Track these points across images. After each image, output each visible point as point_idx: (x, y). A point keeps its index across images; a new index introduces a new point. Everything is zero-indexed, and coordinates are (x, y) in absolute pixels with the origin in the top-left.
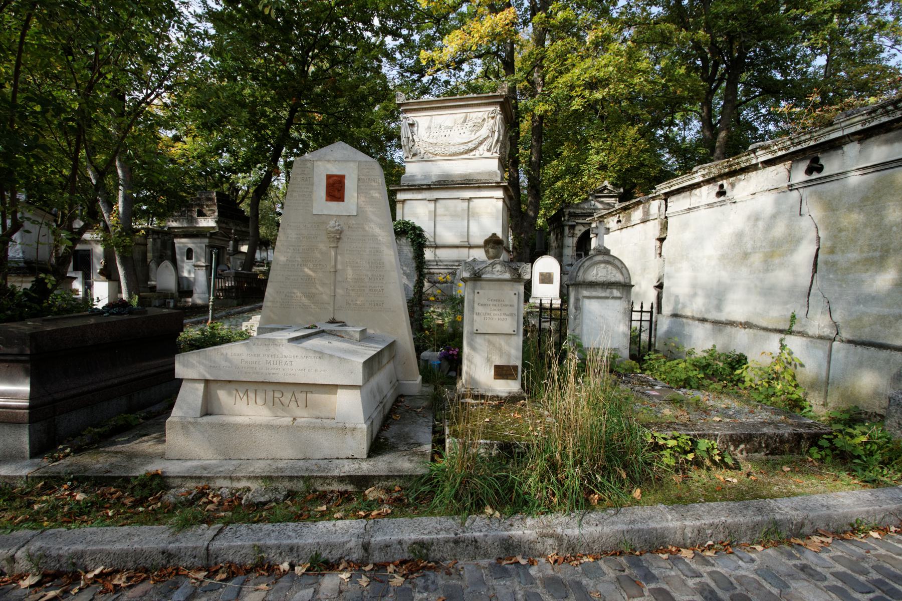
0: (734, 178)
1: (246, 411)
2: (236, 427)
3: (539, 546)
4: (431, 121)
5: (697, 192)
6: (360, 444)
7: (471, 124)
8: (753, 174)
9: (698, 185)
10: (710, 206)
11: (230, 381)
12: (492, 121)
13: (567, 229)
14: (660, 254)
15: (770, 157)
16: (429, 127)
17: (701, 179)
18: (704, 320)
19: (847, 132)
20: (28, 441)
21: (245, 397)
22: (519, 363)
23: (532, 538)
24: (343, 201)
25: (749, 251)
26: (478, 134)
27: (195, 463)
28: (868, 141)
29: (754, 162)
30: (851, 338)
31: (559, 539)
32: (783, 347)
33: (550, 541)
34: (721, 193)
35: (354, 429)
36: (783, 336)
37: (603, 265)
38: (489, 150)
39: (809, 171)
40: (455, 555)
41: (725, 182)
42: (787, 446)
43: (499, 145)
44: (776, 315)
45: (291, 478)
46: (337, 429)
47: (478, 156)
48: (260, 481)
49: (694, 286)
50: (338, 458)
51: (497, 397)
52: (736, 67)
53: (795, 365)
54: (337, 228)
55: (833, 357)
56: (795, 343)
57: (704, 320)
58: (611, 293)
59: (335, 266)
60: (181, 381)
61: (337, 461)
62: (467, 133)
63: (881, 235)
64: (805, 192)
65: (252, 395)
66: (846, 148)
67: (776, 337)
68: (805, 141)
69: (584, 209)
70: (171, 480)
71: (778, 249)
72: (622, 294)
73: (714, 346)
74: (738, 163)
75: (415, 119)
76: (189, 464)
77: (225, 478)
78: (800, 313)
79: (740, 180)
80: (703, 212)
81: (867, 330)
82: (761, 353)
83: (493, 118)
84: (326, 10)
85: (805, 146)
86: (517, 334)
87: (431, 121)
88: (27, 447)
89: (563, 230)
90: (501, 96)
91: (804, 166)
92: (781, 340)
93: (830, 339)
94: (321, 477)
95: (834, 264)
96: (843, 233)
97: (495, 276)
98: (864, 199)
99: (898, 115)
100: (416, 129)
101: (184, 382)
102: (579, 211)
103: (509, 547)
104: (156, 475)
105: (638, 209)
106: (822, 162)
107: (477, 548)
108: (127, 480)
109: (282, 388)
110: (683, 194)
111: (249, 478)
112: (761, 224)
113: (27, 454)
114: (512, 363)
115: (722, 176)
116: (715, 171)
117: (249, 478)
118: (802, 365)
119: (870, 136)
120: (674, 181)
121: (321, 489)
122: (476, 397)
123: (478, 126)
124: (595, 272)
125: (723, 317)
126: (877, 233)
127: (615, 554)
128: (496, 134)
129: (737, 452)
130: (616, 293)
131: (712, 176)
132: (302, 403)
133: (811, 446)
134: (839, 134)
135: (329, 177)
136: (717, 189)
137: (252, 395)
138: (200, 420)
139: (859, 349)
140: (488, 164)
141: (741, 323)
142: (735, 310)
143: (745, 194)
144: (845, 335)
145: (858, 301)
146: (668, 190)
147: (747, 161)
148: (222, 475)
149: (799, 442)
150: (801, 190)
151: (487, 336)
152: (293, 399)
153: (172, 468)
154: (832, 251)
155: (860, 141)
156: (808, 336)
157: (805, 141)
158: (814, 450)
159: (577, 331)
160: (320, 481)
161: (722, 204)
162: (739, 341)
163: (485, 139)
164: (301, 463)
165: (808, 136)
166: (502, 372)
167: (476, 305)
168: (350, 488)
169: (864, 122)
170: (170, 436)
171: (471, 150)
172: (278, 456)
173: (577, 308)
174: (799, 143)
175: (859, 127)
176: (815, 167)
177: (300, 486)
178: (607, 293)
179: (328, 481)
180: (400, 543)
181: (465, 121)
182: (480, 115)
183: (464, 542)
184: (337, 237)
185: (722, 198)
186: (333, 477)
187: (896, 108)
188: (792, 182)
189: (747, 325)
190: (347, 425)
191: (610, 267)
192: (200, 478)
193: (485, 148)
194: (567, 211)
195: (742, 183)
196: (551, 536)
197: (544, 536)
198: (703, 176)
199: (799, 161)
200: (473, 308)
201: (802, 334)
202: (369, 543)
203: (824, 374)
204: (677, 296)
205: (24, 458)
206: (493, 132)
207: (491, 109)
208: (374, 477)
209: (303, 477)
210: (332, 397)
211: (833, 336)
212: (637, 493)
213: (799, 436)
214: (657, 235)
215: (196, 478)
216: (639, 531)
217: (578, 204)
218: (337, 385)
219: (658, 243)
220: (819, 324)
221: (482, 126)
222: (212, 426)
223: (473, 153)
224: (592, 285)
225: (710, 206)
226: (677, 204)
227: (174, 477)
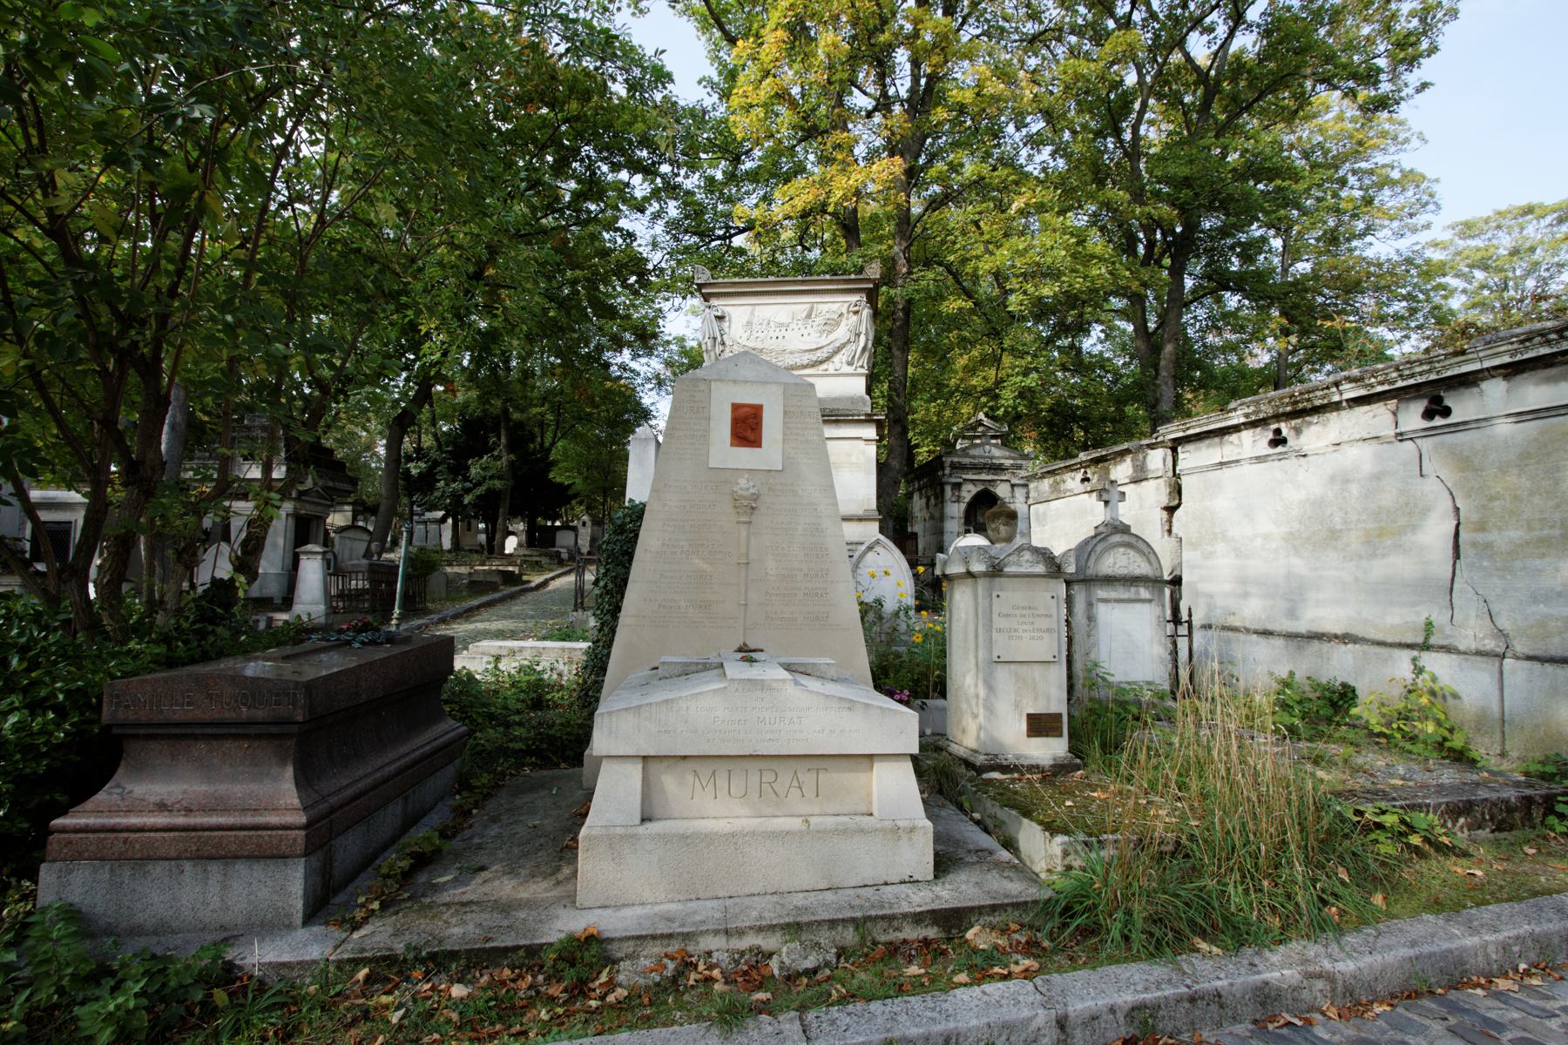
0: (1299, 421)
1: (714, 810)
2: (709, 838)
3: (1305, 995)
4: (752, 313)
5: (1234, 437)
6: (918, 855)
7: (819, 320)
8: (1333, 416)
9: (1236, 429)
10: (1260, 459)
11: (685, 757)
12: (855, 318)
13: (948, 489)
14: (1170, 531)
15: (1363, 392)
16: (749, 323)
17: (1243, 420)
18: (1266, 633)
19: (1487, 364)
20: (300, 893)
21: (711, 785)
22: (1063, 709)
23: (1294, 982)
24: (759, 445)
25: (1339, 527)
26: (832, 337)
27: (647, 910)
28: (1519, 378)
29: (1336, 398)
30: (1531, 653)
31: (1330, 978)
32: (1419, 671)
33: (1320, 984)
34: (1278, 440)
35: (912, 830)
36: (1415, 653)
37: (1122, 550)
38: (850, 364)
39: (1428, 415)
40: (1193, 1023)
41: (1283, 426)
42: (1517, 815)
43: (866, 355)
44: (1400, 619)
45: (833, 923)
46: (883, 830)
47: (831, 371)
48: (779, 934)
49: (1243, 581)
50: (886, 884)
51: (1038, 767)
52: (1182, 248)
53: (1444, 697)
54: (752, 491)
55: (1506, 682)
56: (1435, 663)
57: (1266, 633)
58: (1138, 593)
59: (747, 555)
60: (599, 760)
61: (888, 888)
62: (814, 335)
63: (1558, 506)
64: (1426, 444)
65: (722, 782)
66: (1484, 385)
67: (1406, 656)
68: (1421, 374)
69: (974, 457)
70: (615, 946)
71: (1388, 528)
72: (1152, 593)
73: (1292, 674)
74: (1308, 400)
75: (727, 309)
76: (628, 912)
77: (716, 932)
78: (1440, 617)
79: (1310, 424)
80: (1247, 469)
81: (1556, 640)
82: (1380, 681)
83: (856, 313)
84: (545, 126)
85: (1420, 380)
86: (1058, 662)
87: (752, 313)
88: (299, 904)
89: (943, 491)
90: (868, 280)
91: (1419, 407)
92: (1414, 660)
93: (1497, 655)
94: (883, 917)
95: (1488, 546)
96: (1497, 503)
97: (1022, 570)
98: (1525, 456)
99: (1565, 346)
100: (726, 325)
101: (604, 763)
102: (966, 461)
103: (1266, 997)
104: (591, 939)
105: (1123, 461)
106: (1448, 402)
107: (1221, 1006)
108: (533, 951)
109: (775, 764)
110: (1207, 442)
111: (760, 929)
112: (1354, 489)
113: (298, 918)
114: (1053, 710)
115: (1277, 417)
116: (1267, 410)
117: (760, 929)
118: (1455, 696)
119: (1523, 371)
120: (1192, 422)
121: (883, 938)
122: (1004, 769)
123: (832, 324)
124: (1111, 560)
125: (1302, 627)
126: (1551, 503)
127: (1409, 997)
128: (863, 338)
129: (1456, 829)
130: (1144, 593)
131: (1261, 416)
132: (809, 791)
133: (1545, 815)
134: (1476, 366)
135: (736, 407)
136: (1271, 436)
137: (722, 782)
138: (641, 830)
139: (1549, 668)
140: (846, 382)
141: (1336, 637)
142: (1324, 615)
143: (1322, 443)
144: (1520, 647)
145: (1535, 599)
146: (1181, 434)
147: (1324, 397)
148: (711, 927)
149: (1529, 809)
150: (1419, 441)
151: (1013, 667)
152: (795, 783)
153: (610, 923)
154: (1481, 527)
155: (1506, 377)
156: (1459, 652)
157: (1421, 374)
158: (1552, 820)
159: (1093, 656)
160: (882, 924)
161: (1281, 457)
162: (1339, 665)
163: (844, 346)
164: (829, 896)
165: (1425, 367)
166: (1040, 725)
167: (995, 616)
168: (932, 932)
169: (1513, 353)
170: (587, 862)
171: (821, 362)
172: (784, 888)
173: (1091, 618)
174: (1412, 376)
175: (1507, 359)
176: (1437, 409)
177: (849, 936)
178: (1130, 593)
179: (895, 923)
180: (1112, 1010)
181: (809, 316)
182: (835, 307)
183: (1203, 998)
184: (749, 507)
185: (1280, 449)
186: (905, 916)
187: (1562, 337)
188: (1402, 429)
189: (1346, 638)
190: (900, 824)
191: (1132, 553)
192: (670, 936)
193: (844, 359)
194: (948, 460)
195: (1313, 428)
196: (1319, 976)
197: (1310, 976)
198: (1247, 415)
199: (1408, 400)
200: (991, 620)
201: (1447, 649)
202: (1066, 1017)
203: (1495, 708)
204: (1211, 596)
205: (290, 927)
206: (858, 335)
207: (854, 298)
208: (971, 909)
209: (853, 920)
210: (861, 777)
211: (1500, 650)
212: (1378, 899)
213: (1528, 801)
214: (1165, 501)
215: (662, 936)
216: (1431, 955)
217: (963, 450)
218: (871, 757)
219: (1165, 515)
220: (1472, 632)
221: (838, 324)
222: (665, 838)
223: (824, 366)
224: (1109, 580)
225: (1260, 459)
226: (1190, 457)
227: (621, 939)
